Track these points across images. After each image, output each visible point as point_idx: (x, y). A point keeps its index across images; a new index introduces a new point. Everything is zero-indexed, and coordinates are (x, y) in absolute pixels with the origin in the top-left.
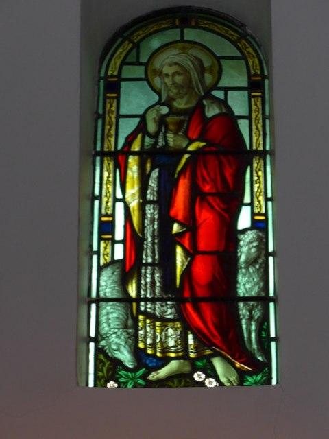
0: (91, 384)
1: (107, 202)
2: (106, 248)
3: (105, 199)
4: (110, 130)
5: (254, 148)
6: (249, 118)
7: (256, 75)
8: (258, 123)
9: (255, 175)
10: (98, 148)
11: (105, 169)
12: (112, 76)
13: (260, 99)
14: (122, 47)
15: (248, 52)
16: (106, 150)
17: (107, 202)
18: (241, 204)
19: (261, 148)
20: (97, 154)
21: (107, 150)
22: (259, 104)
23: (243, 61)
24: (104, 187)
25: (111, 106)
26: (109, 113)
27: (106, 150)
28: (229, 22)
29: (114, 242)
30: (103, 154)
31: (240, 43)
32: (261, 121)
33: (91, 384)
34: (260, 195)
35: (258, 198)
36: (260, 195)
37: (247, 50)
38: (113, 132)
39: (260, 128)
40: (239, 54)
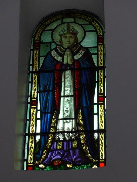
0: (25, 169)
1: (31, 145)
2: (36, 52)
3: (32, 122)
4: (36, 62)
5: (100, 129)
6: (97, 54)
7: (100, 35)
8: (102, 151)
9: (99, 88)
10: (27, 132)
11: (34, 59)
12: (37, 40)
13: (102, 46)
14: (41, 28)
15: (97, 26)
16: (31, 132)
17: (31, 157)
18: (93, 114)
19: (103, 128)
20: (27, 135)
21: (32, 132)
22: (102, 48)
23: (95, 32)
24: (30, 150)
25: (33, 112)
26: (35, 55)
27: (31, 132)
28: (86, 98)
29: (37, 111)
30: (33, 72)
31: (93, 22)
32: (102, 55)
33: (25, 169)
34: (101, 86)
35: (101, 141)
36: (102, 86)
37: (97, 25)
38: (34, 124)
39: (100, 119)
40: (93, 29)
